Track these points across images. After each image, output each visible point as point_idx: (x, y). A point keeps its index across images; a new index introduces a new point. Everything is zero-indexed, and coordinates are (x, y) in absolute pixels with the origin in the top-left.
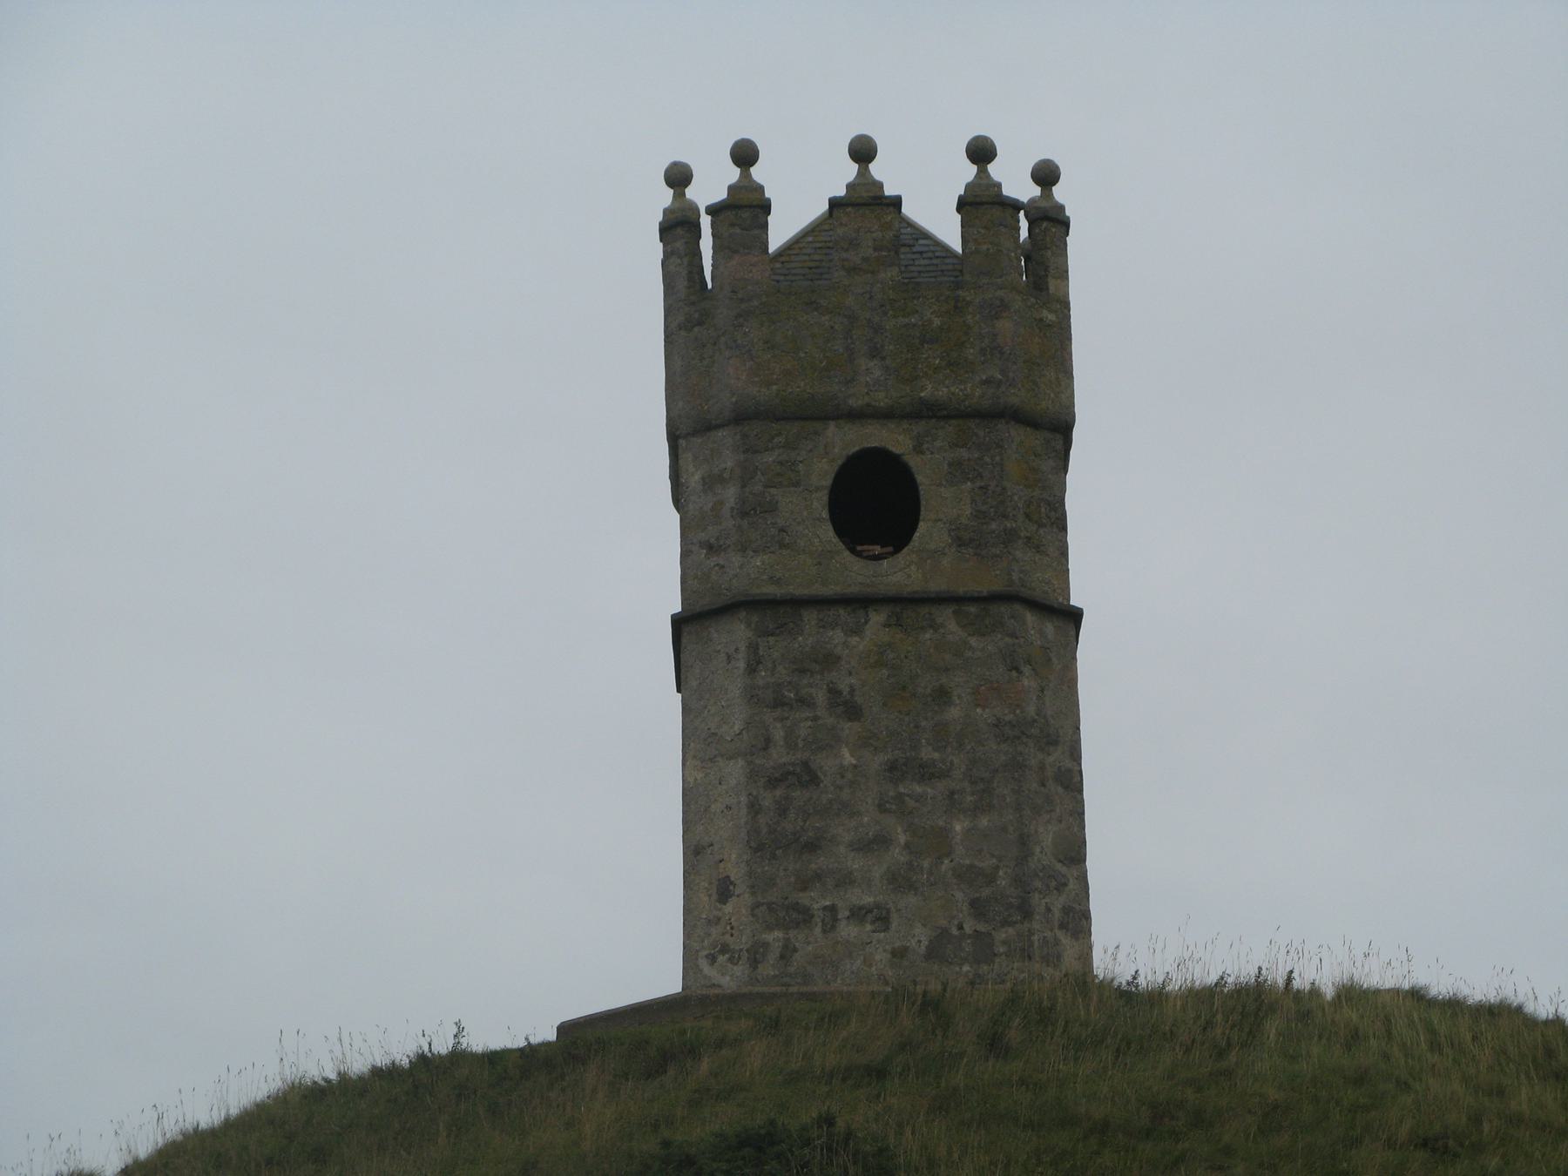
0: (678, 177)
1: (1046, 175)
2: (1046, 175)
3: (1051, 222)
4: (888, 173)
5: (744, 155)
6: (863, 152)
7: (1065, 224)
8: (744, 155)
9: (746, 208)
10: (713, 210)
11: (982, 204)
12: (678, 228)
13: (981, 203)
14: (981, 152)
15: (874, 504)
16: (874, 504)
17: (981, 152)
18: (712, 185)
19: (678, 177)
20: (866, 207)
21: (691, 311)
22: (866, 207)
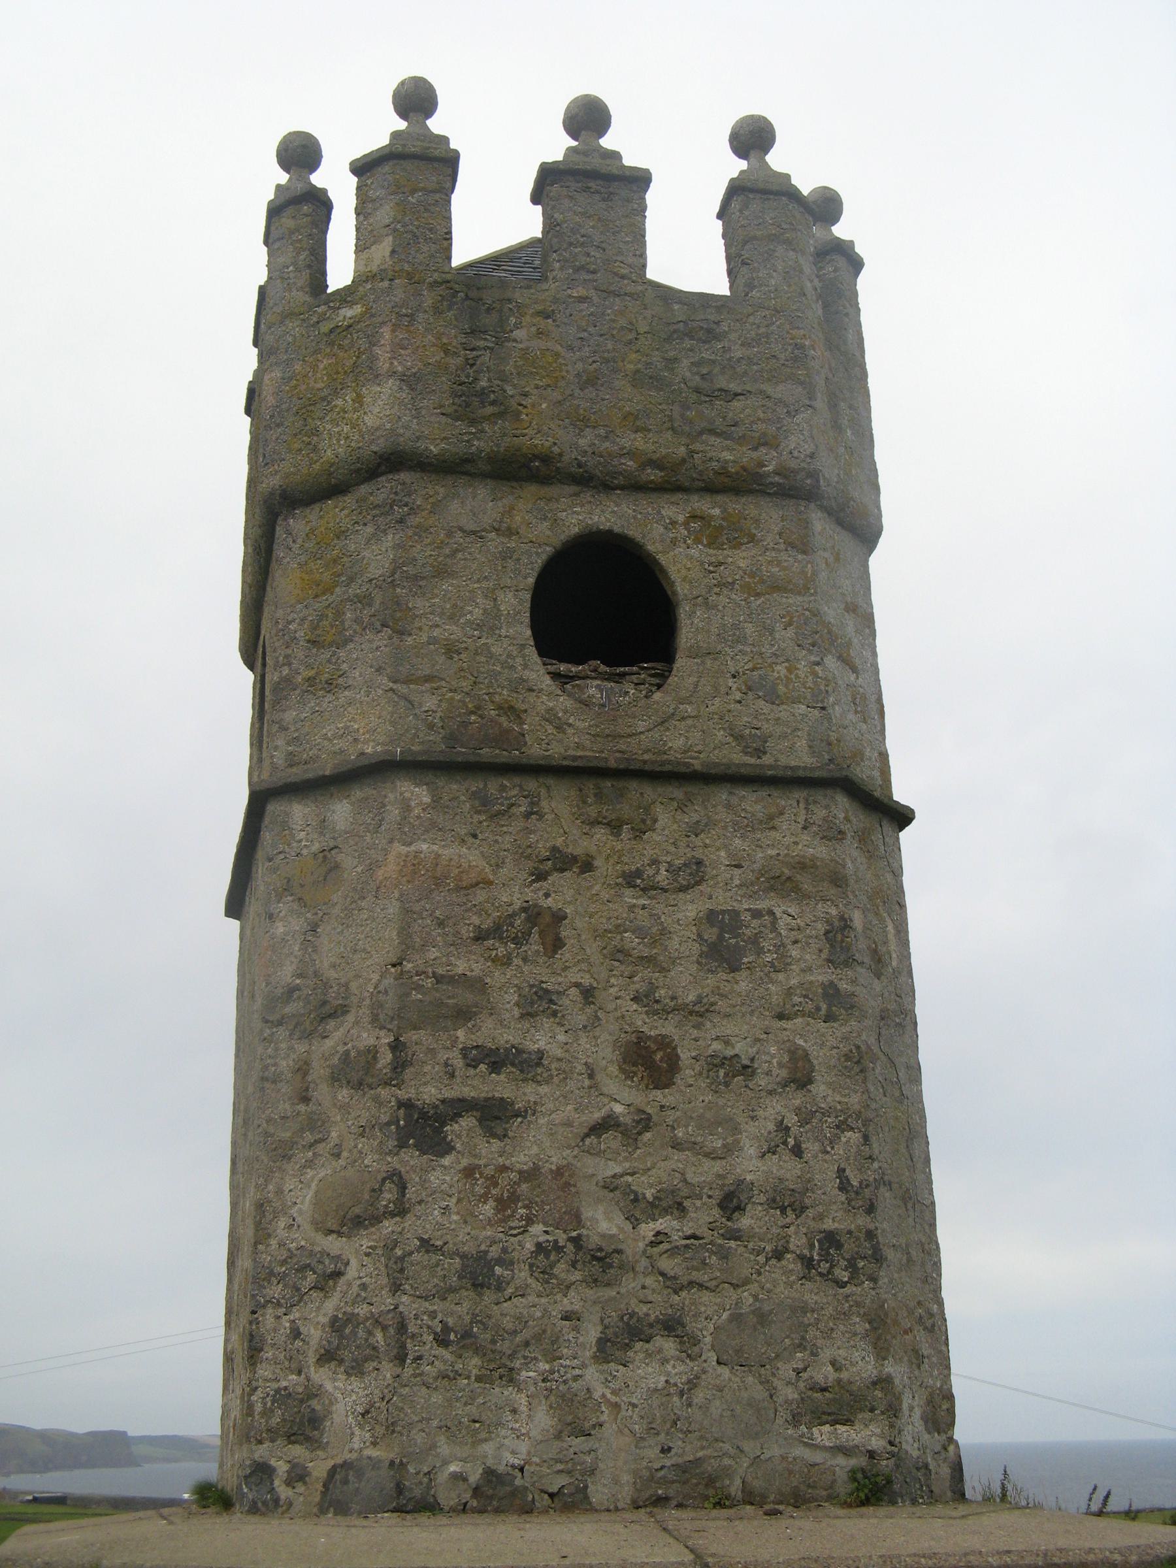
0: (300, 154)
4: (624, 141)
6: (588, 118)
7: (857, 264)
9: (413, 171)
10: (362, 168)
11: (770, 192)
12: (297, 216)
14: (752, 138)
15: (606, 610)
16: (606, 610)
20: (591, 187)
21: (292, 310)
22: (591, 187)
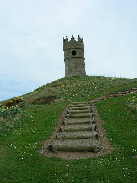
1: (82, 37)
2: (82, 37)
3: (82, 39)
5: (67, 36)
6: (73, 36)
8: (67, 36)
9: (67, 39)
12: (64, 40)
13: (79, 38)
14: (79, 36)
15: (74, 53)
16: (74, 53)
17: (79, 36)
18: (65, 38)
19: (64, 38)
